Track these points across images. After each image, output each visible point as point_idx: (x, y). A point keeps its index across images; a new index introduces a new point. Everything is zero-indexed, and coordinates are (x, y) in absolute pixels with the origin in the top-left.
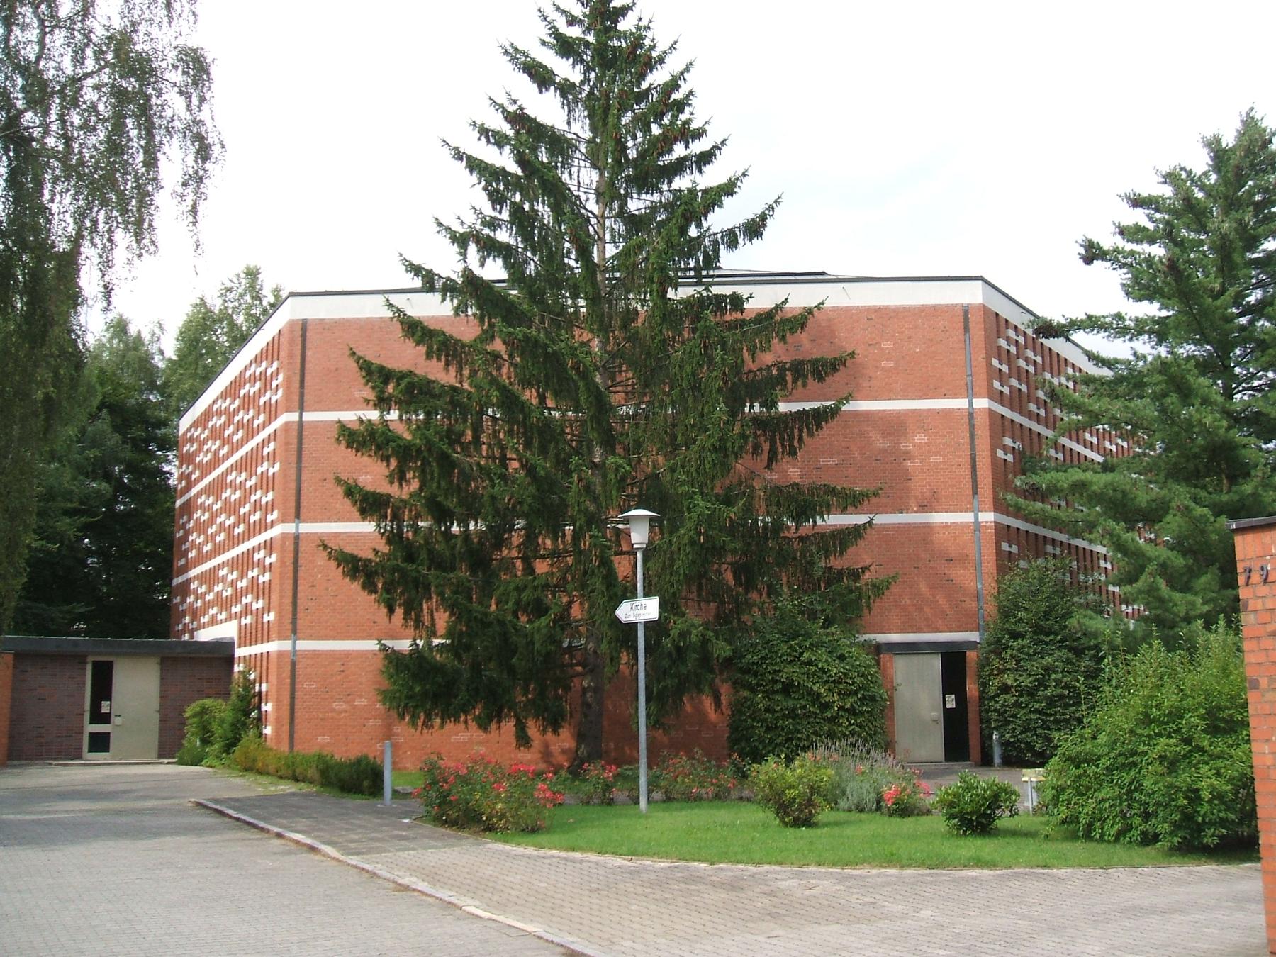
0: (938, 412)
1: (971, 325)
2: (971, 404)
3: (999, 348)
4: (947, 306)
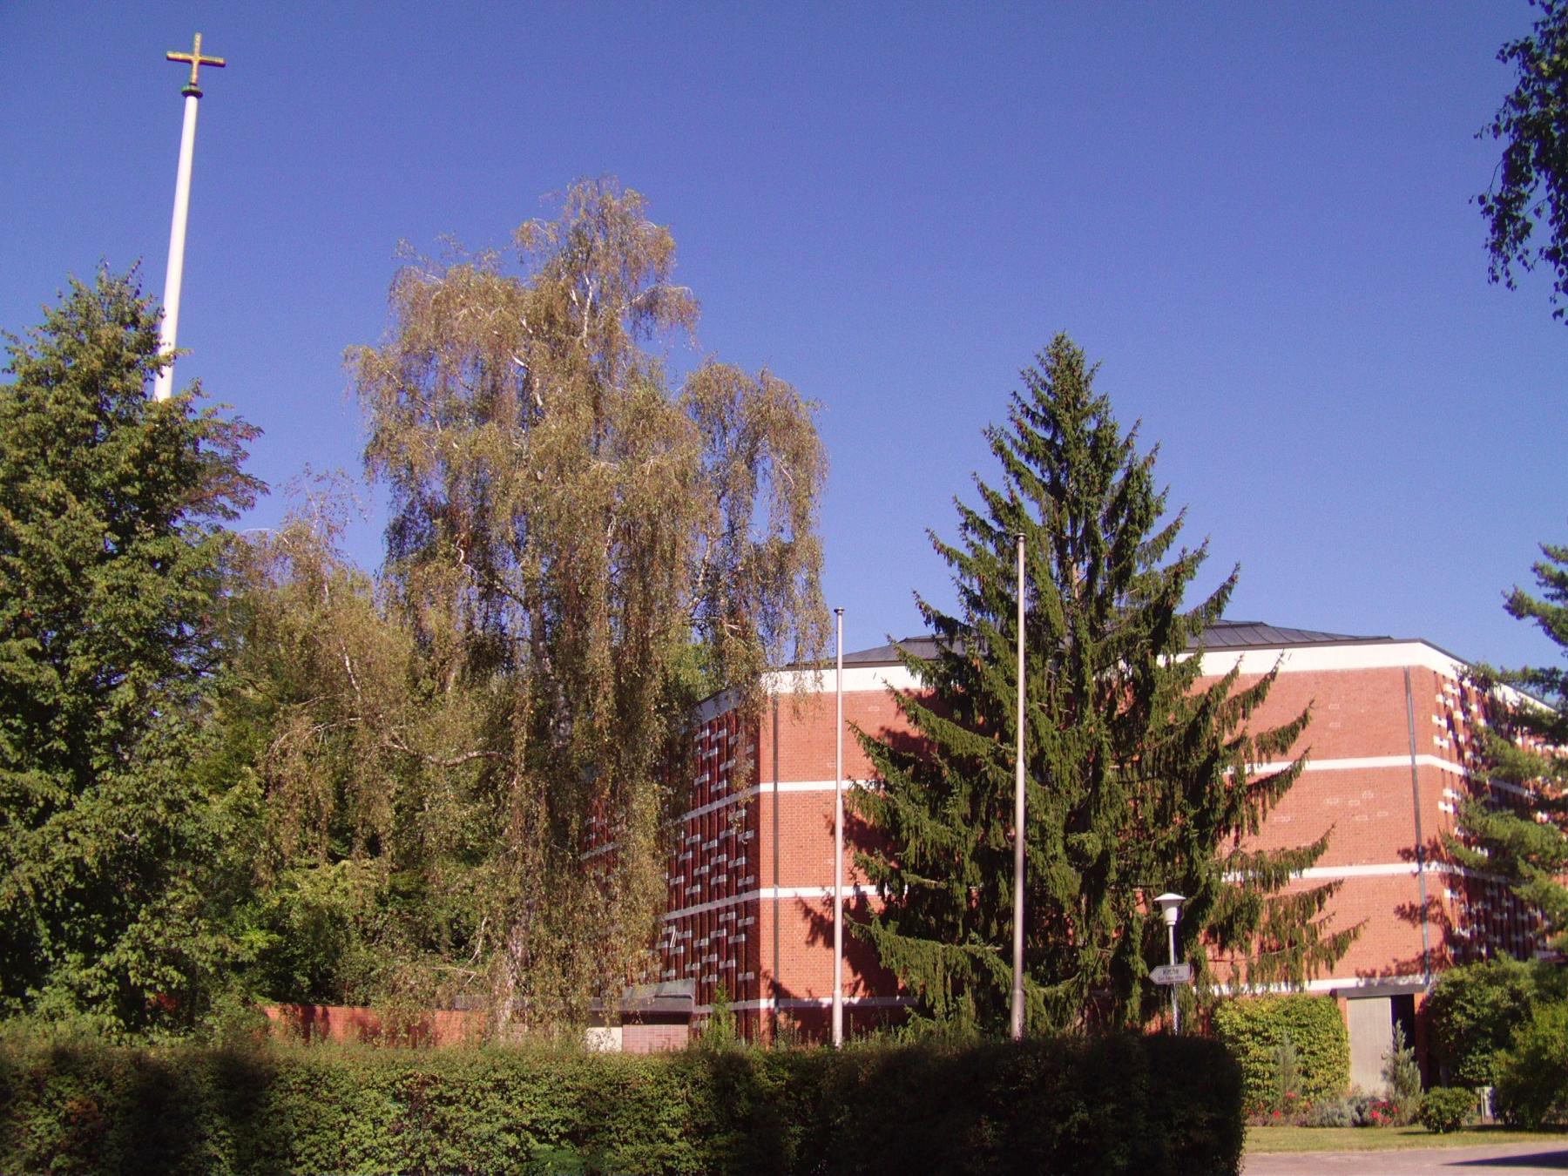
0: (1384, 770)
1: (1412, 685)
2: (1413, 761)
3: (1438, 705)
4: (1390, 669)
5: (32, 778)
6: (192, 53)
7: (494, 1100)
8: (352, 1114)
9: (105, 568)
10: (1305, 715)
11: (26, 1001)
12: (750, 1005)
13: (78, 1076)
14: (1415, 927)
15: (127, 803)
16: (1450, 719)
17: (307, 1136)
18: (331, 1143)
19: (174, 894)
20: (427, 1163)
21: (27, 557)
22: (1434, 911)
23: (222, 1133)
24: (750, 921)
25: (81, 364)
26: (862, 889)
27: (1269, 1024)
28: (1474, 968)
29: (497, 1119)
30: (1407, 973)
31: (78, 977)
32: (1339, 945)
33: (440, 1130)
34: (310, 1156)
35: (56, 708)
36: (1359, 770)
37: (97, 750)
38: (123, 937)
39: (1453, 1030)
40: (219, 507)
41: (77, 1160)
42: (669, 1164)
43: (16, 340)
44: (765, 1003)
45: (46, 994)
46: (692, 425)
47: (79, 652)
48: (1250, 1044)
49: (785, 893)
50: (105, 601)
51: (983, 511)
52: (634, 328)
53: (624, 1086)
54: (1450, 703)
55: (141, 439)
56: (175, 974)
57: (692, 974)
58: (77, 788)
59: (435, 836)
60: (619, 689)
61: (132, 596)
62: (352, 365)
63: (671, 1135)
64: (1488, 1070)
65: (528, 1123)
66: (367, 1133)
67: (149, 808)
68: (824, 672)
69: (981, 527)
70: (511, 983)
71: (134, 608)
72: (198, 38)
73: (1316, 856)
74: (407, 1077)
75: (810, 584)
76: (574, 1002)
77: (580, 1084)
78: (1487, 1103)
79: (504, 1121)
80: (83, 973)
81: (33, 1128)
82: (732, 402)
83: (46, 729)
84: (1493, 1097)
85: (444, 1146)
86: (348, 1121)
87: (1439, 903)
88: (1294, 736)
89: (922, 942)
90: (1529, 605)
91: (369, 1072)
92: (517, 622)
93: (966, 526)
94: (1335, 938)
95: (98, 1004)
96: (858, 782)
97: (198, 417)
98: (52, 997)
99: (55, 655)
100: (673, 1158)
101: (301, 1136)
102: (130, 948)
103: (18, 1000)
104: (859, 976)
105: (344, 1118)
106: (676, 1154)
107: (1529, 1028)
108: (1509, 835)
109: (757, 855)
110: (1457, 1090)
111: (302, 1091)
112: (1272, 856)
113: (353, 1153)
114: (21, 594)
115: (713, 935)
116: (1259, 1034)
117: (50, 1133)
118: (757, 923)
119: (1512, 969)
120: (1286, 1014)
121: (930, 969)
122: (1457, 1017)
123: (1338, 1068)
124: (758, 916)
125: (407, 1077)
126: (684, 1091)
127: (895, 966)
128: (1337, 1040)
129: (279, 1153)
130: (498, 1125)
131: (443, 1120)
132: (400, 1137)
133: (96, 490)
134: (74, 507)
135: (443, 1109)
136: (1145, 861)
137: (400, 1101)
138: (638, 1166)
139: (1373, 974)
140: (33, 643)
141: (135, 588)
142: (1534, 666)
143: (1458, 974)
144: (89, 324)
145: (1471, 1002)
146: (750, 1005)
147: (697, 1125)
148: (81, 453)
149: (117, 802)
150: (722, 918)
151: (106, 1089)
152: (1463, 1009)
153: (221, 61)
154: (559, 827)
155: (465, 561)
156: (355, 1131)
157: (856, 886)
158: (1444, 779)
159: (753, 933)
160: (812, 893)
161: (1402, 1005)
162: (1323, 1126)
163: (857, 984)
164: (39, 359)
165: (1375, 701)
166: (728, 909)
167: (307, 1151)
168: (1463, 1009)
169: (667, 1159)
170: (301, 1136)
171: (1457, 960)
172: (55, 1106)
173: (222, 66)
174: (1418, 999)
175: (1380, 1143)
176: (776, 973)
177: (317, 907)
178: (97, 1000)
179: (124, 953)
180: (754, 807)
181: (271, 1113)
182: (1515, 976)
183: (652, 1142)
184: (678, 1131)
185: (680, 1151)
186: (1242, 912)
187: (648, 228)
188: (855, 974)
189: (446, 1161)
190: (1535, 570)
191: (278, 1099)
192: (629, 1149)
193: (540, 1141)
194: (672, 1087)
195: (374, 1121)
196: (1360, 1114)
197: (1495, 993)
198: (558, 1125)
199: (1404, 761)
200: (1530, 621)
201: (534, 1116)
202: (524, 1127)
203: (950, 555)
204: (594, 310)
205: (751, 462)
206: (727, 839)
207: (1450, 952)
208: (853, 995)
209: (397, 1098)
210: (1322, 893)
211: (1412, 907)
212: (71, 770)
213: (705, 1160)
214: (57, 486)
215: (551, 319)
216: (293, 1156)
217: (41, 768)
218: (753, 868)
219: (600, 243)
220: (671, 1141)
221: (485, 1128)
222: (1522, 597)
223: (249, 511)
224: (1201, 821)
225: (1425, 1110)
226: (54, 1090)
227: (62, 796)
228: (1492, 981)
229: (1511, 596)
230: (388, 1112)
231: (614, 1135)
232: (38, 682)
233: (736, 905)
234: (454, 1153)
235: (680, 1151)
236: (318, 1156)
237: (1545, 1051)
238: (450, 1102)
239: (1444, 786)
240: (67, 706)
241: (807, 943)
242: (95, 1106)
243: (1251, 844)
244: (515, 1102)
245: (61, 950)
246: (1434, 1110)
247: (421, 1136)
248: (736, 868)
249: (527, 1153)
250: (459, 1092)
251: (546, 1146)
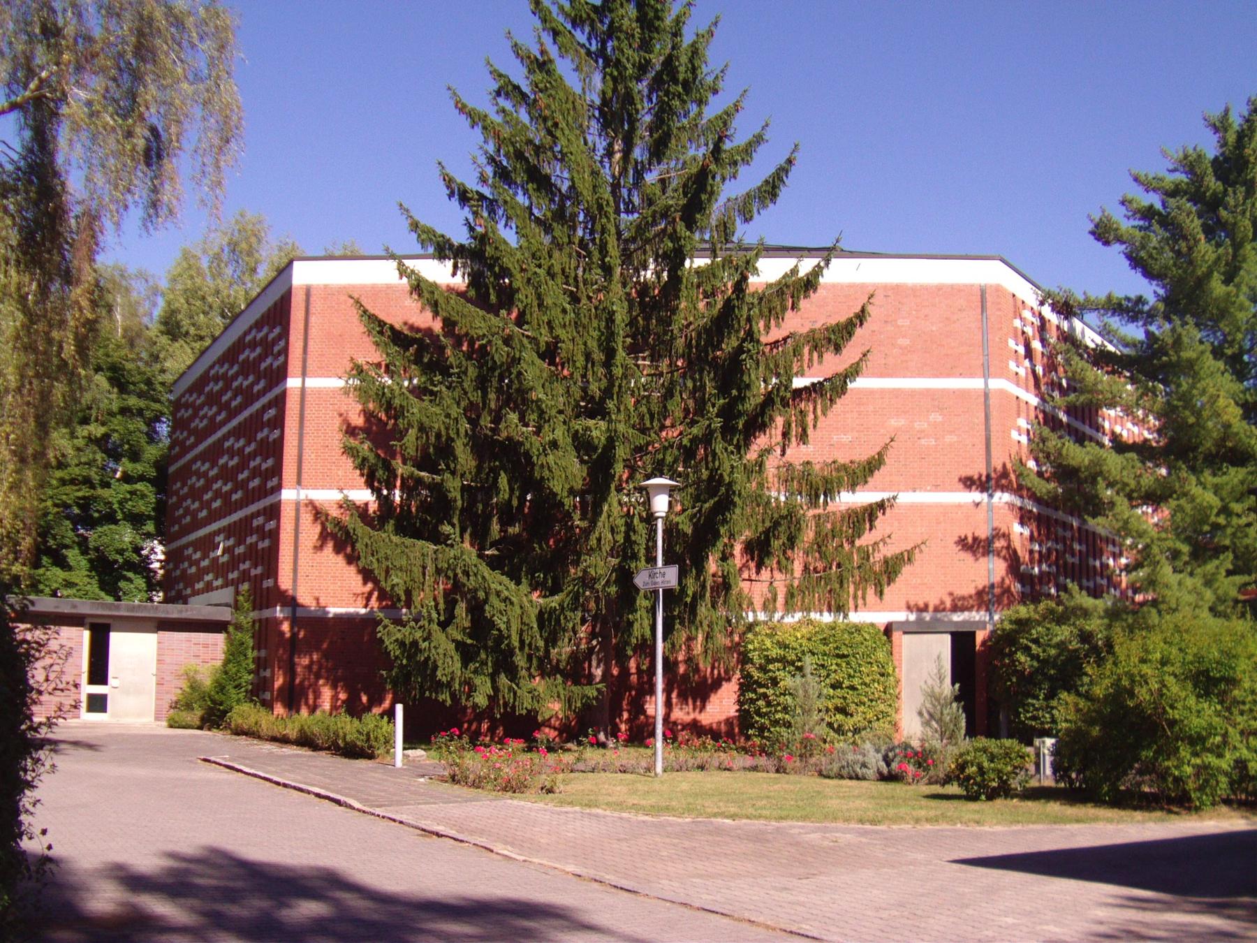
1: (989, 304)
2: (986, 384)
3: (1016, 329)
4: (966, 286)
10: (863, 310)
14: (977, 559)
16: (1027, 346)
22: (1000, 544)
27: (803, 653)
28: (1042, 606)
30: (963, 609)
32: (891, 569)
36: (928, 390)
39: (1016, 672)
48: (780, 674)
51: (519, 75)
54: (1029, 330)
64: (1052, 716)
69: (507, 89)
73: (871, 472)
78: (1048, 759)
84: (1056, 752)
87: (1007, 536)
88: (850, 334)
89: (408, 541)
90: (1117, 229)
93: (498, 93)
94: (886, 562)
107: (1109, 665)
108: (1086, 462)
110: (1008, 742)
112: (822, 469)
116: (792, 663)
119: (1085, 605)
120: (825, 641)
121: (417, 571)
122: (1021, 657)
123: (882, 707)
127: (375, 565)
128: (882, 675)
136: (669, 459)
139: (925, 608)
142: (1119, 294)
143: (1023, 611)
145: (1036, 641)
152: (1027, 649)
158: (1019, 407)
160: (327, 496)
161: (962, 641)
162: (841, 777)
165: (947, 319)
168: (1027, 649)
171: (1023, 599)
174: (980, 636)
180: (280, 402)
182: (1086, 613)
186: (779, 524)
190: (1123, 203)
196: (888, 765)
197: (1063, 633)
199: (977, 383)
200: (1117, 248)
203: (476, 118)
207: (1016, 587)
210: (871, 513)
211: (975, 539)
218: (277, 470)
222: (1109, 221)
224: (728, 414)
225: (962, 767)
228: (1061, 620)
229: (1097, 220)
237: (1132, 694)
239: (1019, 416)
241: (315, 547)
243: (797, 454)
246: (974, 769)
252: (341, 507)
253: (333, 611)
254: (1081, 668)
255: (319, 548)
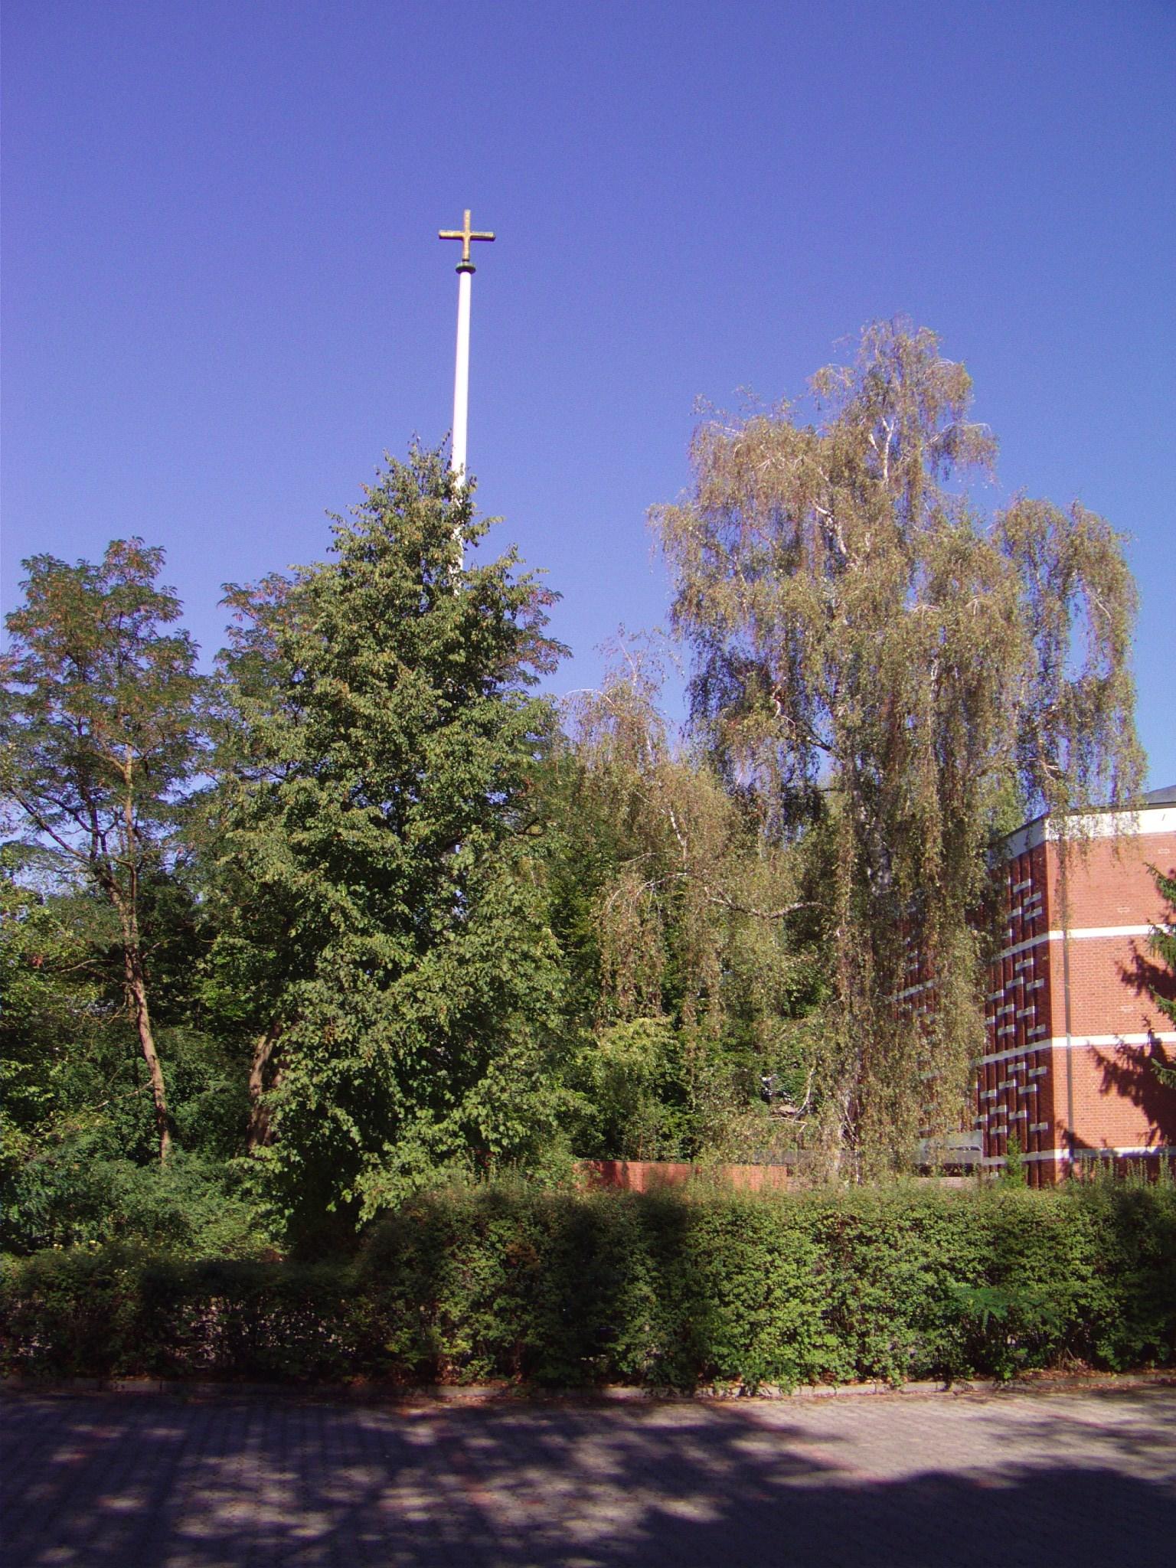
5: (378, 941)
6: (462, 229)
7: (913, 1239)
8: (776, 1254)
9: (435, 736)
11: (383, 1154)
12: (1044, 1155)
13: (517, 1220)
15: (474, 962)
17: (735, 1276)
18: (757, 1283)
19: (515, 1051)
20: (849, 1302)
21: (367, 727)
23: (654, 1274)
24: (1042, 1070)
25: (402, 537)
26: (1157, 1036)
29: (916, 1259)
31: (430, 1132)
33: (860, 1270)
34: (737, 1296)
35: (399, 872)
37: (437, 912)
38: (471, 1094)
40: (520, 674)
41: (519, 1300)
42: (1083, 1302)
43: (339, 520)
44: (1060, 1154)
45: (400, 1149)
46: (1007, 562)
47: (418, 818)
49: (1078, 1041)
50: (442, 767)
52: (933, 469)
53: (1037, 1223)
55: (465, 607)
56: (520, 1128)
57: (979, 1125)
58: (420, 949)
59: (763, 988)
60: (945, 835)
61: (467, 761)
62: (655, 523)
63: (1084, 1273)
65: (946, 1261)
66: (792, 1273)
67: (494, 966)
68: (1140, 812)
70: (840, 1133)
71: (470, 773)
72: (468, 214)
74: (827, 1218)
75: (1124, 722)
76: (902, 1150)
77: (996, 1222)
79: (923, 1260)
80: (436, 1127)
81: (477, 1270)
82: (1043, 538)
83: (388, 894)
85: (864, 1285)
86: (773, 1261)
91: (790, 1213)
92: (826, 771)
95: (449, 1158)
96: (1158, 926)
97: (514, 583)
98: (407, 1152)
99: (396, 822)
100: (1086, 1296)
101: (729, 1277)
102: (479, 1103)
103: (376, 1155)
104: (1155, 1125)
105: (769, 1258)
106: (1090, 1292)
109: (1047, 1004)
111: (728, 1232)
113: (778, 1293)
114: (363, 764)
115: (1001, 1085)
117: (493, 1275)
118: (1050, 1073)
124: (1050, 1066)
125: (827, 1218)
126: (1096, 1228)
129: (708, 1294)
130: (917, 1264)
131: (864, 1259)
132: (822, 1277)
133: (424, 659)
134: (407, 675)
135: (864, 1249)
137: (820, 1241)
138: (1053, 1304)
140: (373, 811)
141: (469, 753)
144: (408, 499)
146: (1044, 1155)
147: (1110, 1262)
148: (409, 623)
149: (462, 961)
150: (1011, 1068)
151: (542, 1233)
153: (491, 235)
154: (885, 979)
155: (782, 713)
156: (781, 1271)
157: (1150, 1033)
159: (1046, 1085)
160: (1105, 1042)
163: (1153, 1133)
164: (362, 538)
166: (1017, 1059)
167: (736, 1291)
169: (1081, 1296)
170: (729, 1277)
172: (497, 1250)
173: (492, 239)
175: (197, 1484)
176: (1071, 1123)
177: (617, 1064)
178: (449, 1154)
179: (473, 1106)
181: (699, 1255)
183: (1065, 1279)
184: (1090, 1269)
185: (1093, 1289)
187: (944, 364)
188: (1151, 1123)
189: (867, 1301)
191: (701, 1237)
192: (1045, 1288)
193: (957, 1280)
194: (1084, 1225)
195: (797, 1261)
198: (975, 1263)
201: (951, 1255)
202: (943, 1266)
204: (894, 454)
205: (1063, 595)
206: (1014, 988)
208: (1149, 1144)
209: (817, 1240)
212: (413, 933)
213: (1118, 1299)
214: (388, 657)
215: (850, 464)
216: (721, 1295)
217: (385, 931)
218: (1044, 1016)
219: (896, 383)
220: (1083, 1279)
221: (905, 1267)
223: (551, 675)
226: (496, 1233)
227: (408, 958)
230: (811, 1252)
231: (1029, 1273)
232: (382, 848)
233: (1026, 1055)
234: (876, 1292)
235: (1093, 1289)
236: (746, 1296)
238: (869, 1241)
240: (408, 870)
241: (1101, 1091)
242: (533, 1249)
244: (933, 1241)
245: (412, 1107)
247: (842, 1276)
248: (1025, 1017)
249: (945, 1292)
250: (878, 1231)
251: (963, 1285)
252: (1118, 1051)
253: (1121, 1151)
254: (361, 1160)
255: (1105, 1091)
